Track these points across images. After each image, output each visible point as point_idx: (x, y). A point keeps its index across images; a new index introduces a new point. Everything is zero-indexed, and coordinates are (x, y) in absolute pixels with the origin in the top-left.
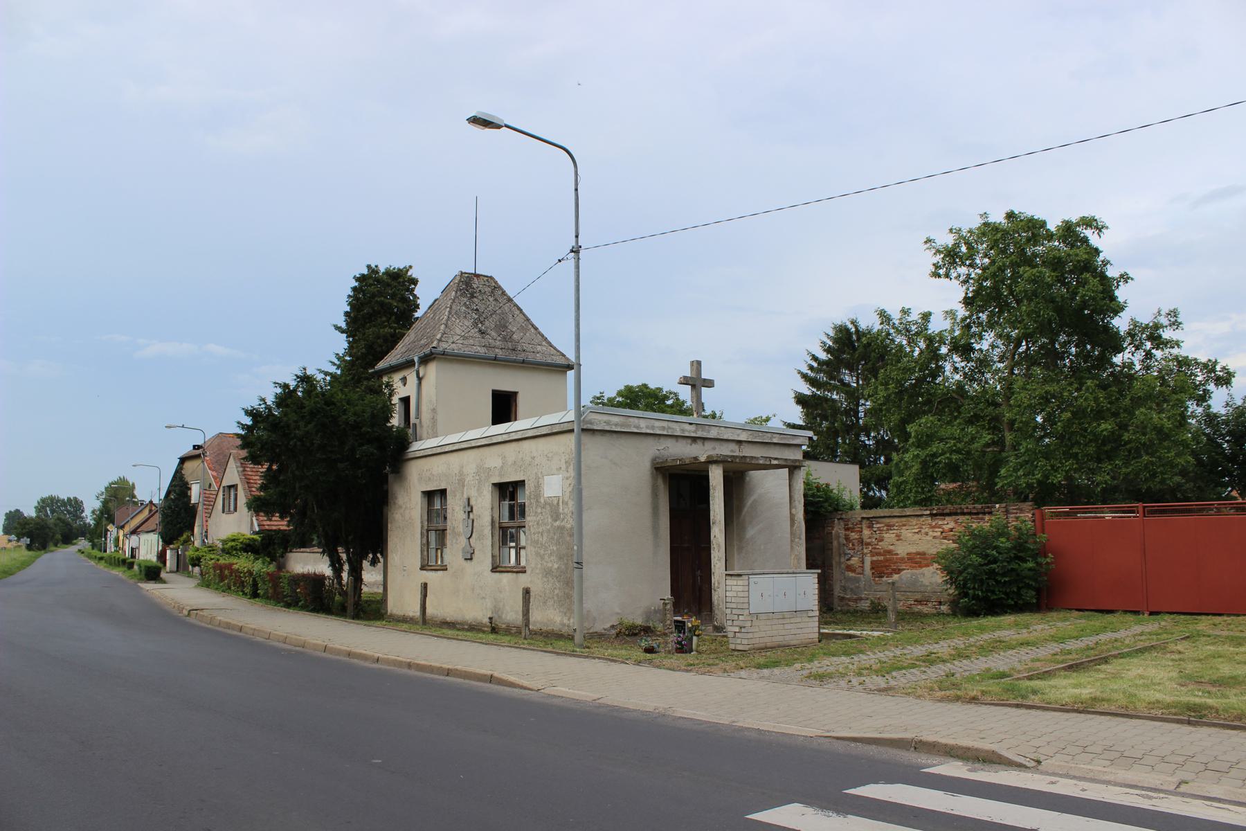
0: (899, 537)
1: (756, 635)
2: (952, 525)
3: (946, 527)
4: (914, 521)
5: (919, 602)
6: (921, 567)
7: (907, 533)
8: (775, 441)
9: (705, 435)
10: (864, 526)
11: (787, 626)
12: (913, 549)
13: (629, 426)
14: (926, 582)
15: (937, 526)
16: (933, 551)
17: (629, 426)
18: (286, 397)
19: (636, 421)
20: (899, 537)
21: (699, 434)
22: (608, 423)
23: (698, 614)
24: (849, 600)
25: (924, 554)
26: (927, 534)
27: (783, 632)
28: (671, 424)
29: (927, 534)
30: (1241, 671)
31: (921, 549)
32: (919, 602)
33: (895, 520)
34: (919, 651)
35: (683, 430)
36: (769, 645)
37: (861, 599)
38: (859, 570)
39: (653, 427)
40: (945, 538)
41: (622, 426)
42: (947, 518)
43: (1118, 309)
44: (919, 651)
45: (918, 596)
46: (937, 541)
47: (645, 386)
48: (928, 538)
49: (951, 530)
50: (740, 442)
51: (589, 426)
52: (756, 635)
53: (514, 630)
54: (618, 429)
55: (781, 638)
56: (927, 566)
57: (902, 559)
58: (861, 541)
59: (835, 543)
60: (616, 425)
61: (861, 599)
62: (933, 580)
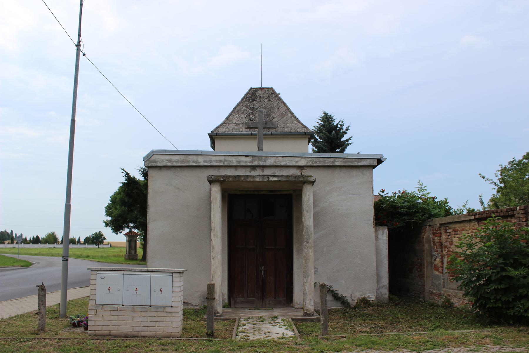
1: (98, 323)
9: (261, 163)
10: (443, 231)
11: (136, 319)
13: (189, 162)
19: (195, 157)
21: (256, 163)
22: (169, 161)
23: (87, 305)
24: (435, 294)
27: (133, 324)
28: (227, 158)
36: (114, 333)
38: (440, 270)
39: (210, 161)
41: (182, 162)
47: (504, 170)
50: (301, 167)
51: (154, 164)
54: (179, 164)
55: (130, 329)
58: (441, 244)
59: (426, 246)
60: (177, 162)
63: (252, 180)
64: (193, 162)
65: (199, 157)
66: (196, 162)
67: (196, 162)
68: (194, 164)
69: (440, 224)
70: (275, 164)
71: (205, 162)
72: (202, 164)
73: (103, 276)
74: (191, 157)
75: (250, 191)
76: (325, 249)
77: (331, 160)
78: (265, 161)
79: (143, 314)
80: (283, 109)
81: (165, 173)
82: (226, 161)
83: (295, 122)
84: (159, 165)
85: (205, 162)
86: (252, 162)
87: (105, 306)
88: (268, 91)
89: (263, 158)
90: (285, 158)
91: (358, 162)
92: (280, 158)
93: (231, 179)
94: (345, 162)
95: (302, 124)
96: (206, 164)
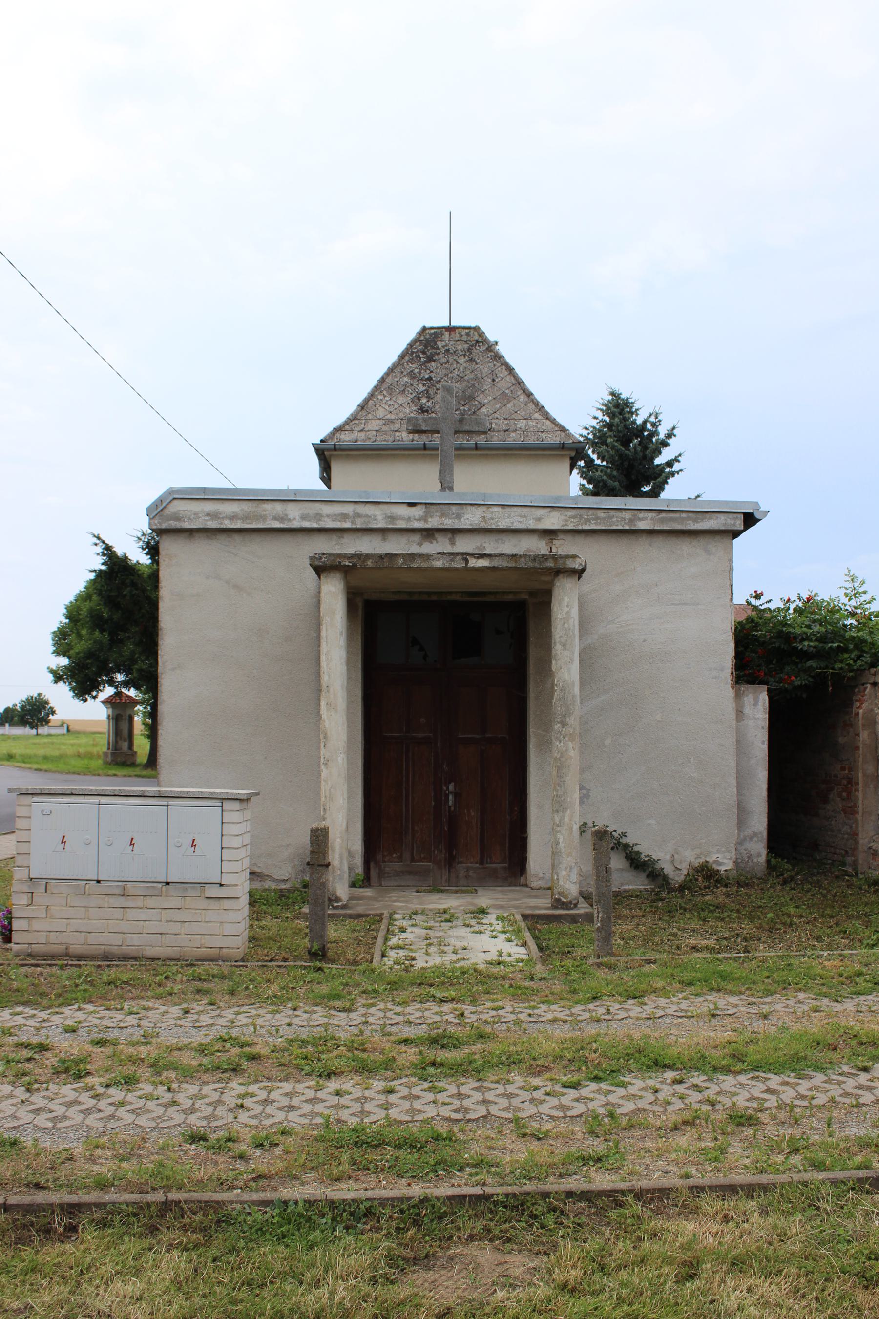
1: (36, 925)
8: (642, 525)
13: (264, 518)
17: (264, 518)
18: (27, 699)
19: (279, 507)
21: (434, 522)
22: (214, 516)
27: (125, 926)
34: (114, 772)
35: (392, 518)
36: (75, 949)
39: (318, 517)
41: (597, 504)
43: (636, 413)
44: (114, 772)
50: (549, 534)
51: (173, 524)
52: (36, 925)
54: (238, 525)
55: (116, 939)
60: (233, 518)
63: (424, 565)
64: (275, 518)
65: (291, 506)
66: (281, 519)
67: (281, 519)
68: (277, 525)
70: (483, 525)
71: (304, 518)
72: (296, 524)
73: (47, 807)
74: (268, 506)
75: (420, 593)
76: (608, 742)
77: (627, 515)
78: (459, 517)
79: (151, 902)
80: (505, 383)
81: (202, 548)
82: (357, 515)
83: (537, 415)
84: (186, 525)
85: (304, 518)
86: (424, 519)
87: (53, 883)
88: (468, 334)
89: (454, 508)
90: (508, 509)
91: (696, 521)
92: (496, 509)
93: (370, 563)
94: (662, 521)
95: (554, 421)
96: (307, 524)
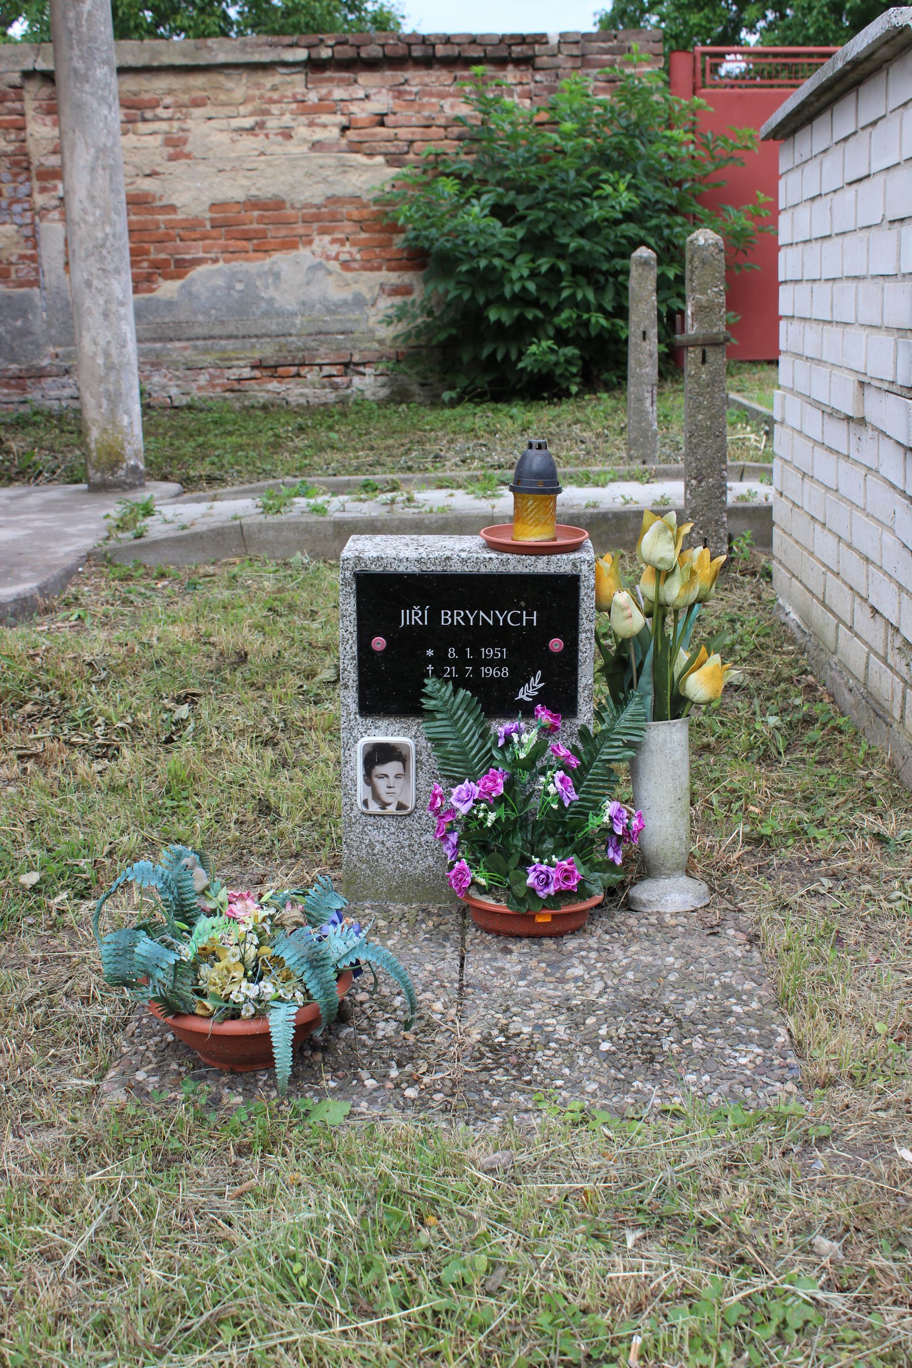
0: (176, 147)
2: (382, 102)
3: (362, 112)
4: (239, 87)
5: (268, 369)
6: (264, 250)
7: (207, 131)
10: (30, 106)
12: (234, 190)
14: (286, 300)
15: (326, 106)
16: (313, 193)
20: (176, 147)
25: (278, 204)
26: (287, 134)
29: (287, 134)
30: (15, 638)
31: (266, 186)
32: (268, 369)
33: (161, 83)
37: (40, 374)
40: (355, 148)
42: (366, 79)
45: (267, 351)
46: (329, 159)
48: (295, 148)
49: (380, 120)
53: (27, 232)
56: (289, 245)
57: (193, 225)
61: (40, 374)
62: (314, 292)
69: (28, 75)
